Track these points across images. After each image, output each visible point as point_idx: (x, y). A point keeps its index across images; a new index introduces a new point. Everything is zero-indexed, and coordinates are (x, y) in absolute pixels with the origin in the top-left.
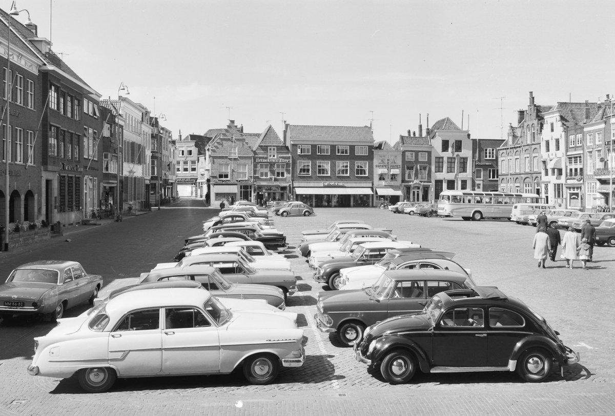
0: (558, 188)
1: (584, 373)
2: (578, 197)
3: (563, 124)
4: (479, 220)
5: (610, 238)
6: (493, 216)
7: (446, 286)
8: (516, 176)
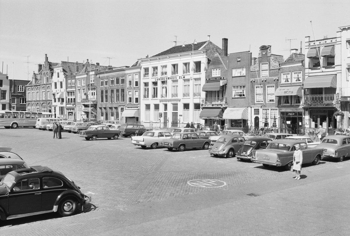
0: (62, 109)
1: (92, 207)
2: (73, 114)
3: (64, 73)
4: (16, 128)
5: (93, 136)
6: (24, 125)
7: (9, 167)
8: (37, 102)
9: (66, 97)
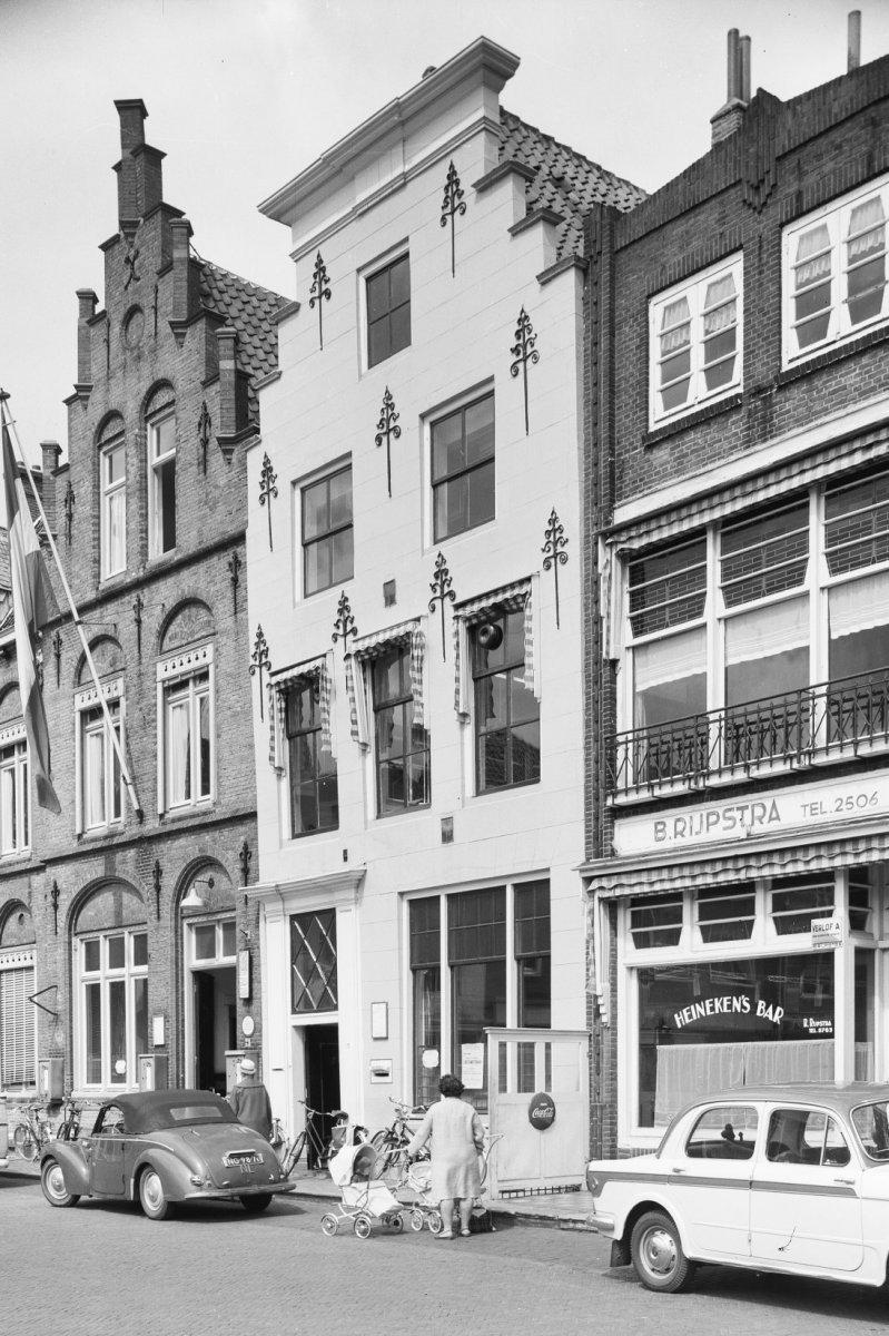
9: (601, 674)
